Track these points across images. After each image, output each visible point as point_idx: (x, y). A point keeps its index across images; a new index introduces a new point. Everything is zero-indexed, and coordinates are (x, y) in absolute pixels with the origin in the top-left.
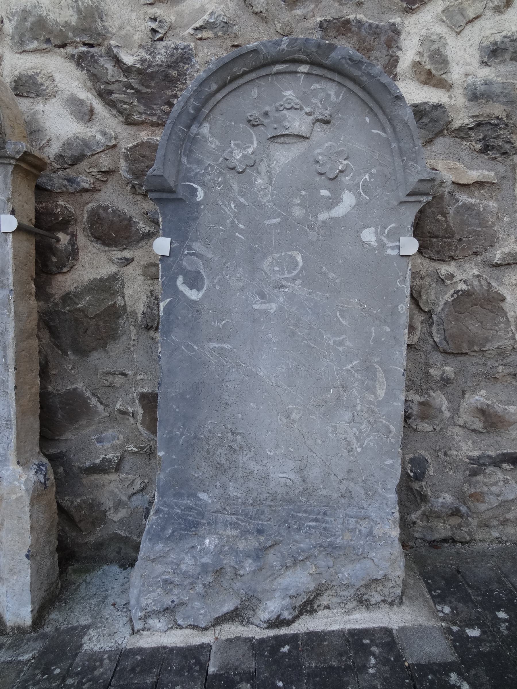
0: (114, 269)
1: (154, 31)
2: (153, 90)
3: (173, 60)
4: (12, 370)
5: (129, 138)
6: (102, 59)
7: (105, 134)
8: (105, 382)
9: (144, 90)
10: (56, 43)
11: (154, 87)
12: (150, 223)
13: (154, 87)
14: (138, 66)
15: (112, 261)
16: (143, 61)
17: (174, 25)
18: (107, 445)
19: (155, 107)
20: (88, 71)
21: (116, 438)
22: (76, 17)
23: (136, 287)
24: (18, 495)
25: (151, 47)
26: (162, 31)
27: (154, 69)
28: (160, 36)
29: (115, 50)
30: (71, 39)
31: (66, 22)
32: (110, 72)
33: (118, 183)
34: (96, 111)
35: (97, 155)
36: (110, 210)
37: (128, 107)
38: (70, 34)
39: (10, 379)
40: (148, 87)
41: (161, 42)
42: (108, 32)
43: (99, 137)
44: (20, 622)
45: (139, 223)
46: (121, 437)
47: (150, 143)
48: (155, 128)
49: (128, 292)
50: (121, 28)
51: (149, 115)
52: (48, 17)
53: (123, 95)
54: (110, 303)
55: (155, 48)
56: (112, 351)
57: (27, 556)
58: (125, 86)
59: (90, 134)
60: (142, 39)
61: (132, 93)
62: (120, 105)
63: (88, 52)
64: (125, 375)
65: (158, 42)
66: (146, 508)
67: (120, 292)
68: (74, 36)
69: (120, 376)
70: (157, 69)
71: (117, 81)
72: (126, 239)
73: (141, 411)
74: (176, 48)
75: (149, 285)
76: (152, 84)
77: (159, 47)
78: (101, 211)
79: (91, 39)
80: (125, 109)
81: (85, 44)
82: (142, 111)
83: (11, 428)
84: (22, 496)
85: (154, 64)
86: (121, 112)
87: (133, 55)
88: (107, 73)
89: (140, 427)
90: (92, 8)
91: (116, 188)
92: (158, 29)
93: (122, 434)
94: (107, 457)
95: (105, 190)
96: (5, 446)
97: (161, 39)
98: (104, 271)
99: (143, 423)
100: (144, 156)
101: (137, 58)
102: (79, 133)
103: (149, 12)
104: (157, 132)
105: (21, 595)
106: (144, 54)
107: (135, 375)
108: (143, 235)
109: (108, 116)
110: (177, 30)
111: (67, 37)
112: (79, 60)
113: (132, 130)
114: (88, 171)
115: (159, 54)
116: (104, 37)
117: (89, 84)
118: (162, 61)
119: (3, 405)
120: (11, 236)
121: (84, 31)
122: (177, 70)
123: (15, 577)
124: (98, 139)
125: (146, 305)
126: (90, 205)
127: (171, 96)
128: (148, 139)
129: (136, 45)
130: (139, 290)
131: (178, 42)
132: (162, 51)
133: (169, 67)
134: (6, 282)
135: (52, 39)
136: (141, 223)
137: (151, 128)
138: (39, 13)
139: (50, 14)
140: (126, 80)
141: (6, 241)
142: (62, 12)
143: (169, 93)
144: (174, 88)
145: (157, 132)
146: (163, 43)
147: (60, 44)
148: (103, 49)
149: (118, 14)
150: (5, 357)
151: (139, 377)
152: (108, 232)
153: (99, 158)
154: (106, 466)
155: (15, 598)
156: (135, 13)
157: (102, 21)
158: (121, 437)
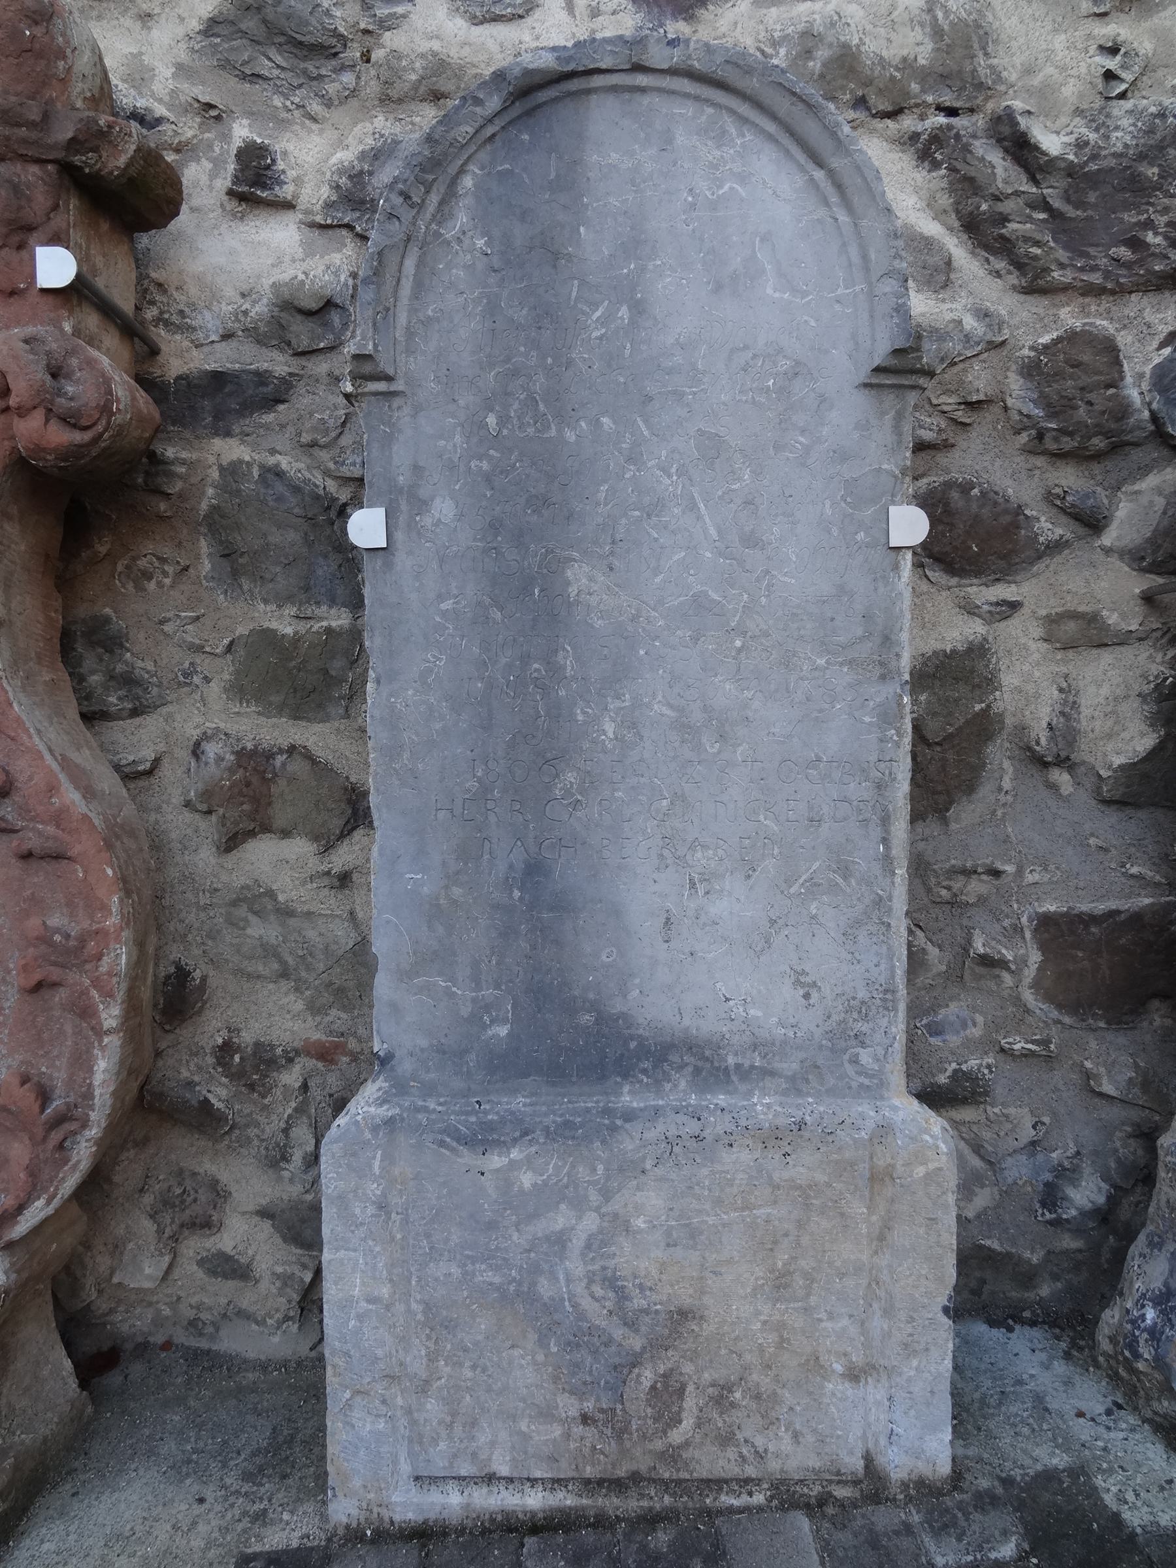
0: (975, 629)
1: (1109, 76)
2: (1090, 212)
3: (1152, 142)
4: (901, 872)
5: (1035, 325)
6: (977, 143)
7: (986, 315)
8: (944, 892)
9: (1070, 212)
10: (881, 107)
11: (1094, 206)
12: (1064, 519)
13: (1094, 206)
14: (1071, 157)
15: (970, 609)
16: (1081, 144)
17: (1153, 62)
18: (954, 1040)
19: (1092, 251)
20: (952, 169)
21: (970, 1023)
22: (929, 46)
23: (1026, 667)
24: (931, 1166)
25: (1100, 113)
26: (1128, 76)
27: (1105, 164)
28: (1123, 87)
29: (1023, 122)
30: (916, 97)
31: (905, 59)
32: (999, 171)
33: (995, 429)
34: (955, 264)
35: (961, 366)
36: (976, 491)
37: (1039, 251)
38: (915, 87)
39: (896, 893)
40: (1080, 205)
41: (1122, 102)
42: (999, 79)
43: (969, 322)
44: (923, 1468)
45: (1038, 520)
46: (980, 1019)
47: (1090, 333)
48: (1087, 300)
49: (1009, 679)
50: (1029, 71)
51: (1082, 269)
52: (863, 49)
53: (1028, 225)
54: (978, 707)
55: (1108, 116)
56: (957, 821)
57: (946, 1310)
58: (1028, 205)
59: (949, 316)
60: (1081, 96)
61: (1043, 221)
62: (1022, 249)
63: (950, 127)
64: (996, 873)
65: (1115, 103)
66: (1047, 1184)
67: (990, 683)
68: (923, 91)
69: (984, 877)
70: (1112, 162)
71: (1017, 193)
72: (1003, 557)
73: (1035, 957)
74: (1162, 115)
75: (1057, 662)
76: (1092, 197)
77: (1116, 112)
78: (955, 495)
79: (957, 99)
80: (1036, 258)
81: (940, 108)
82: (1066, 261)
83: (895, 1009)
84: (940, 1169)
85: (1103, 153)
86: (1019, 266)
87: (1058, 133)
88: (994, 174)
89: (1028, 996)
90: (967, 26)
91: (990, 440)
92: (1119, 72)
93: (981, 1013)
94: (964, 1067)
95: (963, 444)
96: (880, 1051)
97: (1123, 96)
98: (956, 634)
99: (1036, 985)
100: (1077, 365)
101: (1067, 139)
102: (923, 315)
103: (1096, 32)
104: (1093, 308)
105: (928, 1404)
106: (1084, 130)
107: (1020, 872)
108: (1047, 547)
109: (981, 273)
110: (1160, 73)
111: (907, 95)
112: (927, 149)
113: (1037, 305)
114: (935, 402)
115: (1117, 128)
116: (990, 93)
117: (945, 201)
118: (1126, 146)
119: (877, 954)
120: (909, 556)
121: (945, 78)
122: (1159, 166)
123: (915, 1363)
124: (967, 327)
125: (1058, 708)
126: (925, 480)
127: (1136, 224)
128: (1085, 324)
129: (1069, 109)
130: (1037, 674)
131: (1167, 102)
132: (1125, 122)
133: (1142, 157)
134: (894, 663)
135: (872, 99)
136: (1043, 519)
137: (1081, 300)
138: (842, 39)
139: (867, 40)
140: (1034, 190)
141: (896, 567)
142: (893, 36)
143: (1130, 217)
144: (1144, 207)
145: (1093, 308)
146: (1128, 105)
147: (890, 109)
148: (980, 121)
149: (1022, 40)
150: (885, 841)
151: (1030, 878)
152: (963, 542)
153: (965, 370)
154: (965, 1089)
155: (912, 1413)
156: (1063, 37)
157: (986, 54)
158: (980, 1019)
